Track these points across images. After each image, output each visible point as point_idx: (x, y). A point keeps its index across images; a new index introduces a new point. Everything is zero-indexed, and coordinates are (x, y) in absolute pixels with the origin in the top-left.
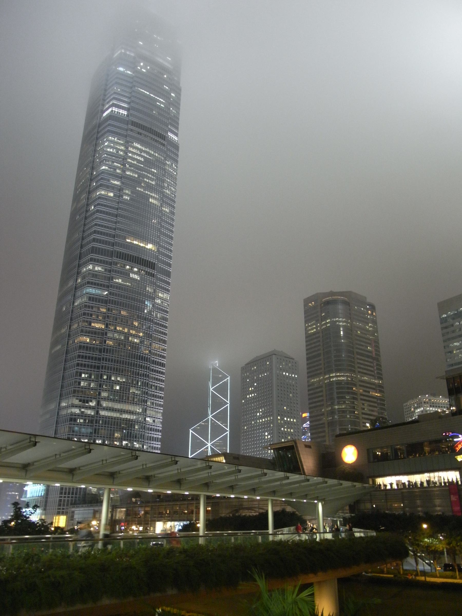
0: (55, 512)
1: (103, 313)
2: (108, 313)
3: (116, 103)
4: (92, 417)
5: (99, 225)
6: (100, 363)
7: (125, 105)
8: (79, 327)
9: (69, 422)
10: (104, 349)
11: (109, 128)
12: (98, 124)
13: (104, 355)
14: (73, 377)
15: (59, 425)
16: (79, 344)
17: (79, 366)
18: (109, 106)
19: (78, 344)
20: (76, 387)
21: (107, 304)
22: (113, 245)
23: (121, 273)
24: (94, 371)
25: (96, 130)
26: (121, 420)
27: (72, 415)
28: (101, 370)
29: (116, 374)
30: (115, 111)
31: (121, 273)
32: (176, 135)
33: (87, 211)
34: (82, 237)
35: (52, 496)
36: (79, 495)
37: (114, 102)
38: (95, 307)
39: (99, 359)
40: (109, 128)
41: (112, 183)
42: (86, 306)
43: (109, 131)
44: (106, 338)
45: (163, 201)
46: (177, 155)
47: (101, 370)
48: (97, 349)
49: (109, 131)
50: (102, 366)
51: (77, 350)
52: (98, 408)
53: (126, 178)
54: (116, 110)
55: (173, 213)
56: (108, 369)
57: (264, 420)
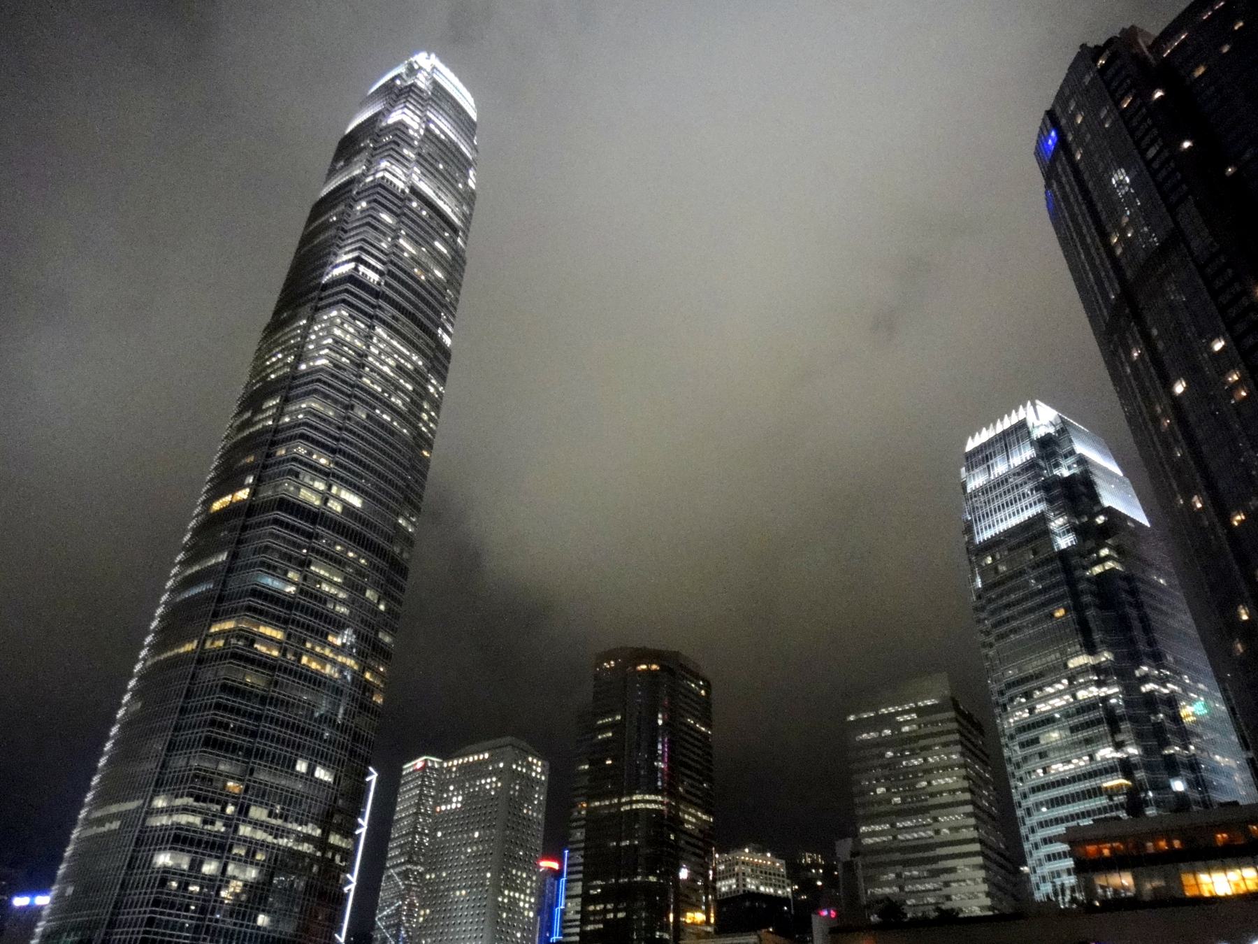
4: (221, 837)
5: (325, 383)
7: (379, 266)
8: (227, 647)
9: (172, 844)
11: (345, 296)
12: (247, 505)
14: (186, 783)
15: (143, 848)
16: (193, 772)
19: (171, 829)
20: (195, 788)
21: (291, 610)
22: (337, 439)
23: (327, 556)
25: (238, 522)
26: (279, 849)
27: (200, 770)
28: (253, 760)
29: (307, 670)
31: (327, 556)
32: (452, 325)
33: (269, 456)
34: (220, 595)
38: (281, 569)
40: (345, 296)
41: (256, 649)
43: (344, 301)
46: (446, 369)
47: (253, 760)
48: (257, 696)
49: (344, 301)
51: (198, 746)
52: (238, 820)
53: (362, 389)
55: (457, 300)
56: (273, 736)
57: (475, 848)
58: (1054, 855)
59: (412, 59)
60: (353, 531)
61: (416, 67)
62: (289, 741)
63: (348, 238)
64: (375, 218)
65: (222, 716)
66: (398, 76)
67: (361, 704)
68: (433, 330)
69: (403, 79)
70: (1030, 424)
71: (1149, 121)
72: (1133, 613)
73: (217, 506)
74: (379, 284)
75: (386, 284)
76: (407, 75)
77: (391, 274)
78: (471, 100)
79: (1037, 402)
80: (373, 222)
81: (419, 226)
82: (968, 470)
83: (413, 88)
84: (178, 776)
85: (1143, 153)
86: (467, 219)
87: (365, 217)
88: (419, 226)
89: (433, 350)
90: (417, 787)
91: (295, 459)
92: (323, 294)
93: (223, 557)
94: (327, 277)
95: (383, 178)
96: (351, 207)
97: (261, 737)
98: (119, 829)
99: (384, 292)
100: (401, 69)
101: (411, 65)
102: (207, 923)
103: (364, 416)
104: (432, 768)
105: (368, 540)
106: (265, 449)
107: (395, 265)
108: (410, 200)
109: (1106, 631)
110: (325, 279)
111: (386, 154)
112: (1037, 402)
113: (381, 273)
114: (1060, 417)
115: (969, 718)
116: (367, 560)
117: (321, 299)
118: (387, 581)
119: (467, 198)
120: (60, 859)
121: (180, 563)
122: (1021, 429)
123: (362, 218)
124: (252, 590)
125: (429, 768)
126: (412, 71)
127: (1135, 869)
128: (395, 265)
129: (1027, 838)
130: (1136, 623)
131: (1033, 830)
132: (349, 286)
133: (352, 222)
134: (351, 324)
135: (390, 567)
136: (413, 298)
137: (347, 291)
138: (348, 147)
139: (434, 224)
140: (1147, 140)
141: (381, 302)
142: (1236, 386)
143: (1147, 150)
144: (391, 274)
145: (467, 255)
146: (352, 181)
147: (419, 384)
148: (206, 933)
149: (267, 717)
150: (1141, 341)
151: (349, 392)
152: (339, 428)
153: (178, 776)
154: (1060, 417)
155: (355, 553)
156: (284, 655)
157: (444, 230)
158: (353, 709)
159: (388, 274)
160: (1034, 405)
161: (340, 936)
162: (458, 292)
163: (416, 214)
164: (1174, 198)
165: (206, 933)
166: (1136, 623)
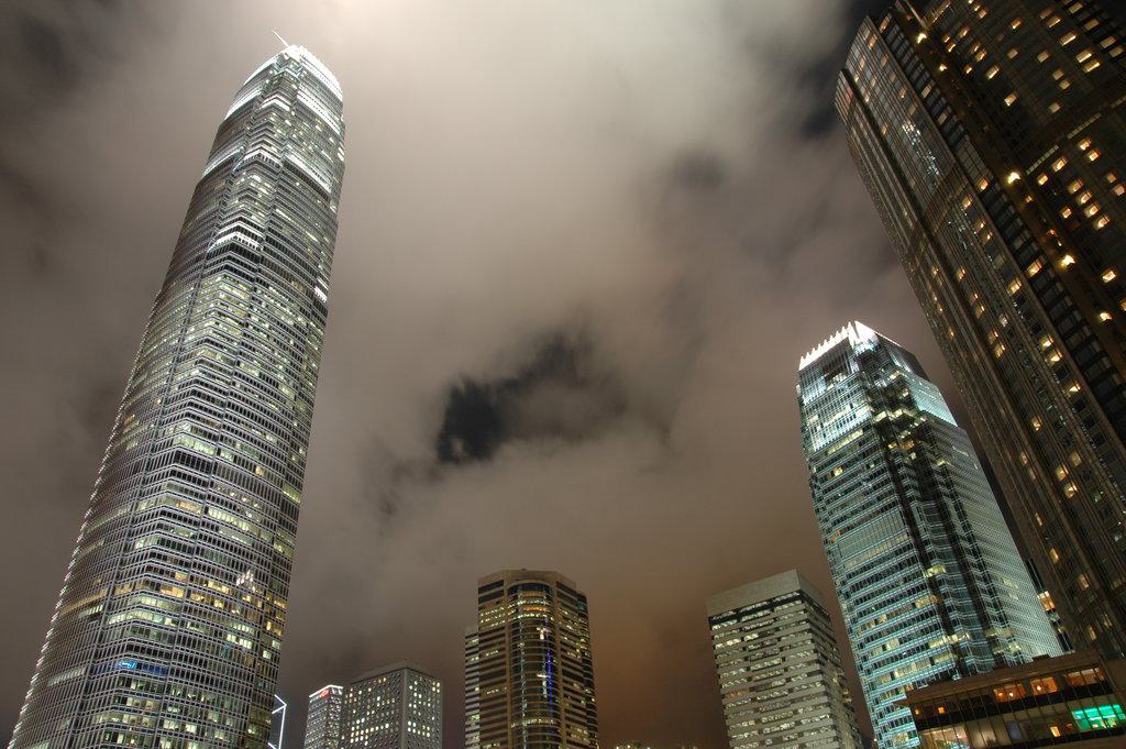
7: (258, 234)
42: (153, 555)
44: (160, 732)
54: (242, 238)
58: (896, 721)
61: (287, 58)
63: (225, 225)
66: (271, 67)
70: (852, 344)
71: (917, 58)
72: (950, 503)
73: (56, 681)
74: (258, 249)
75: (265, 249)
78: (337, 84)
79: (857, 323)
82: (802, 386)
85: (935, 119)
86: (337, 188)
90: (321, 739)
92: (151, 474)
93: (79, 672)
95: (259, 155)
96: (231, 183)
101: (281, 56)
103: (257, 375)
104: (336, 696)
107: (273, 231)
109: (930, 520)
110: (210, 249)
112: (857, 323)
113: (261, 241)
114: (879, 336)
115: (819, 610)
116: (260, 505)
119: (338, 170)
122: (844, 348)
125: (333, 695)
127: (968, 723)
128: (273, 231)
129: (877, 723)
130: (953, 512)
131: (881, 716)
132: (256, 166)
133: (228, 211)
135: (282, 510)
136: (291, 261)
137: (229, 258)
138: (228, 131)
140: (921, 83)
141: (261, 266)
142: (1049, 351)
143: (923, 88)
145: (338, 219)
146: (231, 161)
150: (938, 263)
154: (879, 336)
157: (317, 198)
160: (854, 325)
161: (276, 744)
162: (334, 240)
164: (953, 138)
166: (953, 512)
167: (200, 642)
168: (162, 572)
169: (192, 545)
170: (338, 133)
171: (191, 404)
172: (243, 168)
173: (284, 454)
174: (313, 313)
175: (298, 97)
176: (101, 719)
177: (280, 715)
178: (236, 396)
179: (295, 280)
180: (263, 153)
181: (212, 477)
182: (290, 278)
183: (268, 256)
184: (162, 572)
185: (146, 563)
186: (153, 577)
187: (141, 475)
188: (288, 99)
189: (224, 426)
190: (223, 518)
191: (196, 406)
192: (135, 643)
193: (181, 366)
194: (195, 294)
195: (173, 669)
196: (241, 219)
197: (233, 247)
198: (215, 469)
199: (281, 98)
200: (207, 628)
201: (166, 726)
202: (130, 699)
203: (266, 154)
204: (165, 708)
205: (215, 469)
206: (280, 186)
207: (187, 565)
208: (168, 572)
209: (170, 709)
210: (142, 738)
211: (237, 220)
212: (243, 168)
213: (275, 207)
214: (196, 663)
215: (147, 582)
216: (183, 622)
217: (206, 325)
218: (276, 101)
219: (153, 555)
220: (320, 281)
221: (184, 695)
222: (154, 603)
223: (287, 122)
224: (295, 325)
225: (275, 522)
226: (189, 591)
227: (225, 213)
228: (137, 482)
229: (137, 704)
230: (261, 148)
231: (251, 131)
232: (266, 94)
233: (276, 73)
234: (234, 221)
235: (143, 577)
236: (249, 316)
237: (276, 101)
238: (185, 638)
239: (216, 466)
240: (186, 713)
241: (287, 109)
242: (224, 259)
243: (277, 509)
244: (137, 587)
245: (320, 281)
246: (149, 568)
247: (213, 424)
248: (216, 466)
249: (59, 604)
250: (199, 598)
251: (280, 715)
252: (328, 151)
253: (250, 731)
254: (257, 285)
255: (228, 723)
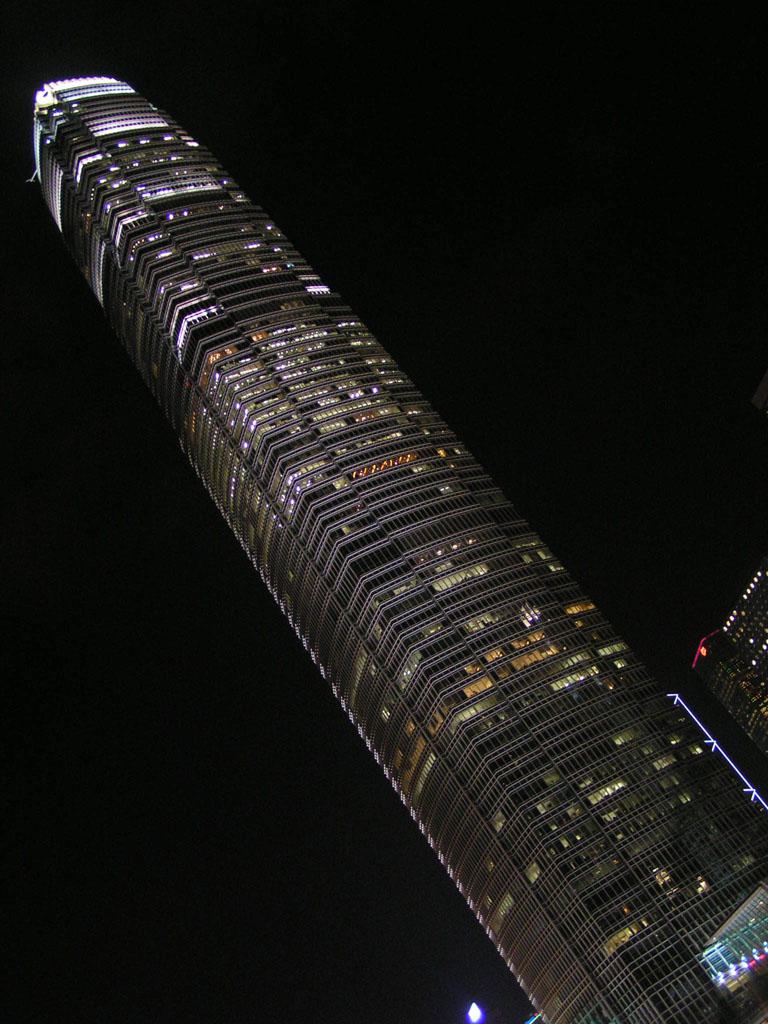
0: (648, 1004)
1: (492, 691)
2: (500, 684)
3: (184, 306)
6: (531, 734)
10: (526, 719)
13: (557, 761)
17: (486, 752)
18: (177, 321)
24: (542, 772)
30: (195, 321)
35: (623, 971)
36: (696, 987)
37: (181, 308)
39: (533, 744)
42: (428, 673)
43: (205, 348)
44: (582, 794)
45: (400, 401)
50: (550, 752)
54: (195, 318)
59: (37, 110)
60: (434, 528)
62: (561, 724)
63: (163, 316)
64: (157, 266)
65: (504, 771)
66: (43, 137)
67: (635, 694)
68: (304, 295)
69: (48, 134)
74: (219, 311)
75: (224, 304)
76: (47, 128)
77: (219, 293)
80: (160, 270)
81: (194, 228)
83: (63, 132)
84: (514, 827)
87: (150, 274)
88: (194, 228)
89: (322, 311)
91: (309, 499)
92: (351, 607)
94: (180, 356)
95: (125, 227)
97: (542, 740)
98: (516, 901)
99: (231, 314)
100: (38, 129)
101: (40, 116)
102: (682, 938)
105: (454, 520)
106: (362, 643)
108: (164, 218)
111: (72, 155)
116: (473, 537)
117: (303, 544)
118: (539, 574)
120: (512, 977)
121: (341, 693)
123: (148, 278)
124: (306, 498)
126: (46, 120)
132: (202, 342)
134: (122, 190)
135: (498, 523)
139: (201, 212)
141: (240, 324)
144: (219, 293)
147: (344, 351)
148: (678, 927)
149: (550, 752)
151: (251, 352)
152: (243, 329)
153: (514, 827)
155: (457, 542)
156: (497, 678)
157: (216, 207)
158: (658, 737)
159: (218, 296)
163: (182, 222)
165: (678, 927)
167: (549, 708)
168: (452, 680)
169: (422, 590)
170: (165, 125)
171: (317, 511)
172: (125, 255)
173: (514, 568)
174: (330, 314)
175: (96, 135)
176: (609, 950)
177: (716, 748)
178: (373, 499)
179: (282, 303)
180: (125, 222)
181: (408, 554)
182: (275, 306)
183: (235, 309)
184: (452, 680)
185: (429, 686)
186: (449, 691)
187: (343, 617)
188: (90, 148)
189: (367, 500)
190: (454, 582)
191: (405, 625)
192: (428, 666)
193: (272, 488)
194: (213, 412)
195: (538, 736)
196: (176, 302)
197: (196, 334)
198: (401, 547)
199: (79, 147)
200: (645, 838)
201: (594, 802)
202: (539, 807)
203: (129, 220)
204: (578, 789)
205: (401, 547)
206: (203, 274)
207: (544, 760)
208: (457, 675)
209: (582, 786)
210: (583, 828)
211: (173, 308)
212: (125, 255)
213: (191, 258)
214: (577, 737)
215: (448, 701)
216: (515, 704)
217: (253, 428)
218: (85, 162)
219: (428, 673)
220: (304, 278)
221: (638, 828)
222: (473, 712)
223: (113, 169)
224: (327, 344)
225: (502, 539)
226: (493, 673)
227: (156, 313)
228: (347, 626)
229: (550, 805)
230: (120, 219)
231: (93, 215)
232: (68, 169)
233: (53, 137)
234: (172, 312)
235: (440, 699)
236: (279, 379)
237: (85, 162)
238: (532, 716)
239: (399, 544)
240: (601, 777)
241: (99, 157)
242: (144, 266)
243: (492, 526)
244: (445, 712)
245: (304, 278)
246: (438, 687)
247: (354, 509)
248: (399, 544)
249: (395, 785)
250: (612, 815)
251: (716, 748)
252: (175, 152)
253: (673, 742)
254: (330, 448)
255: (646, 752)
